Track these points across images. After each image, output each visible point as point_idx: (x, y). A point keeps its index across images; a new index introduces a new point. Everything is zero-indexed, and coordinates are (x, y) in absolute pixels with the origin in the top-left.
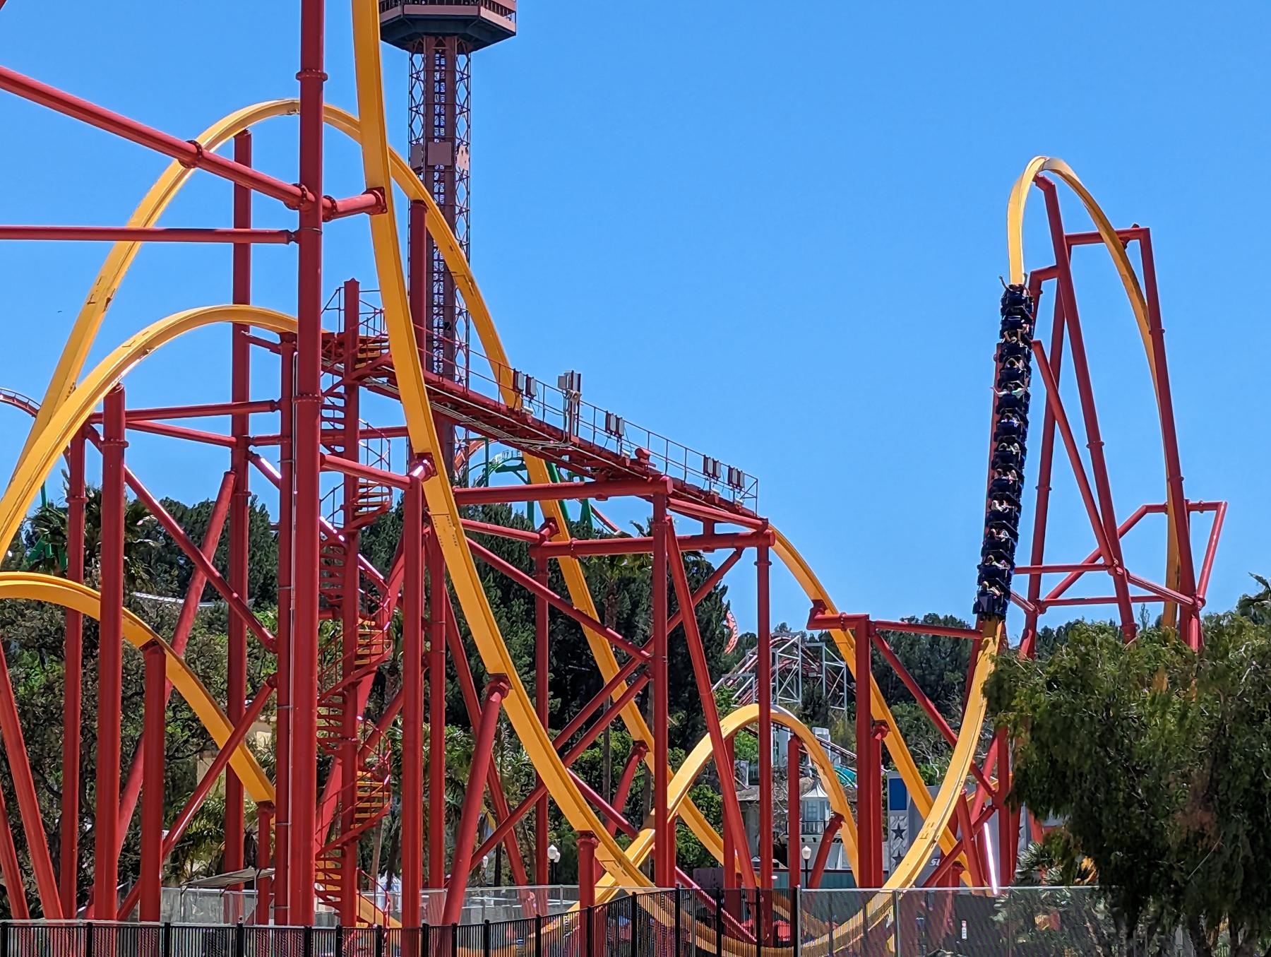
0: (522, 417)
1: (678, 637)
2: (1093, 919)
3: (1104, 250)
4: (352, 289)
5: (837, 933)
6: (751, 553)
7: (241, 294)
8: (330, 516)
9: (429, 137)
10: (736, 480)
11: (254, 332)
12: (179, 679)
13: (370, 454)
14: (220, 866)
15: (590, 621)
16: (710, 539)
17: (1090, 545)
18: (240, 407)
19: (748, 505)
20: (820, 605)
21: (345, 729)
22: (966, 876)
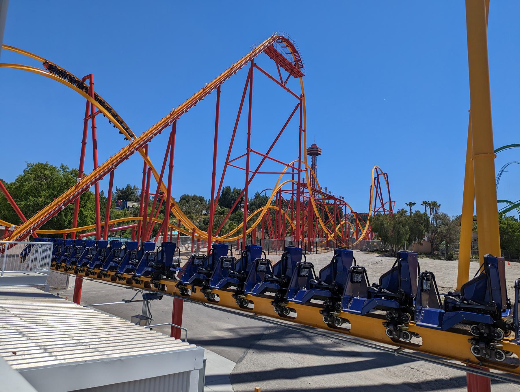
0: (321, 191)
1: (337, 214)
2: (381, 244)
3: (382, 175)
4: (304, 178)
5: (353, 244)
6: (344, 206)
7: (293, 179)
8: (301, 201)
9: (313, 164)
10: (343, 198)
11: (294, 183)
12: (287, 217)
13: (305, 195)
14: (291, 235)
15: (328, 212)
16: (340, 204)
17: (381, 206)
18: (293, 190)
19: (344, 201)
20: (352, 211)
21: (303, 222)
22: (367, 239)
